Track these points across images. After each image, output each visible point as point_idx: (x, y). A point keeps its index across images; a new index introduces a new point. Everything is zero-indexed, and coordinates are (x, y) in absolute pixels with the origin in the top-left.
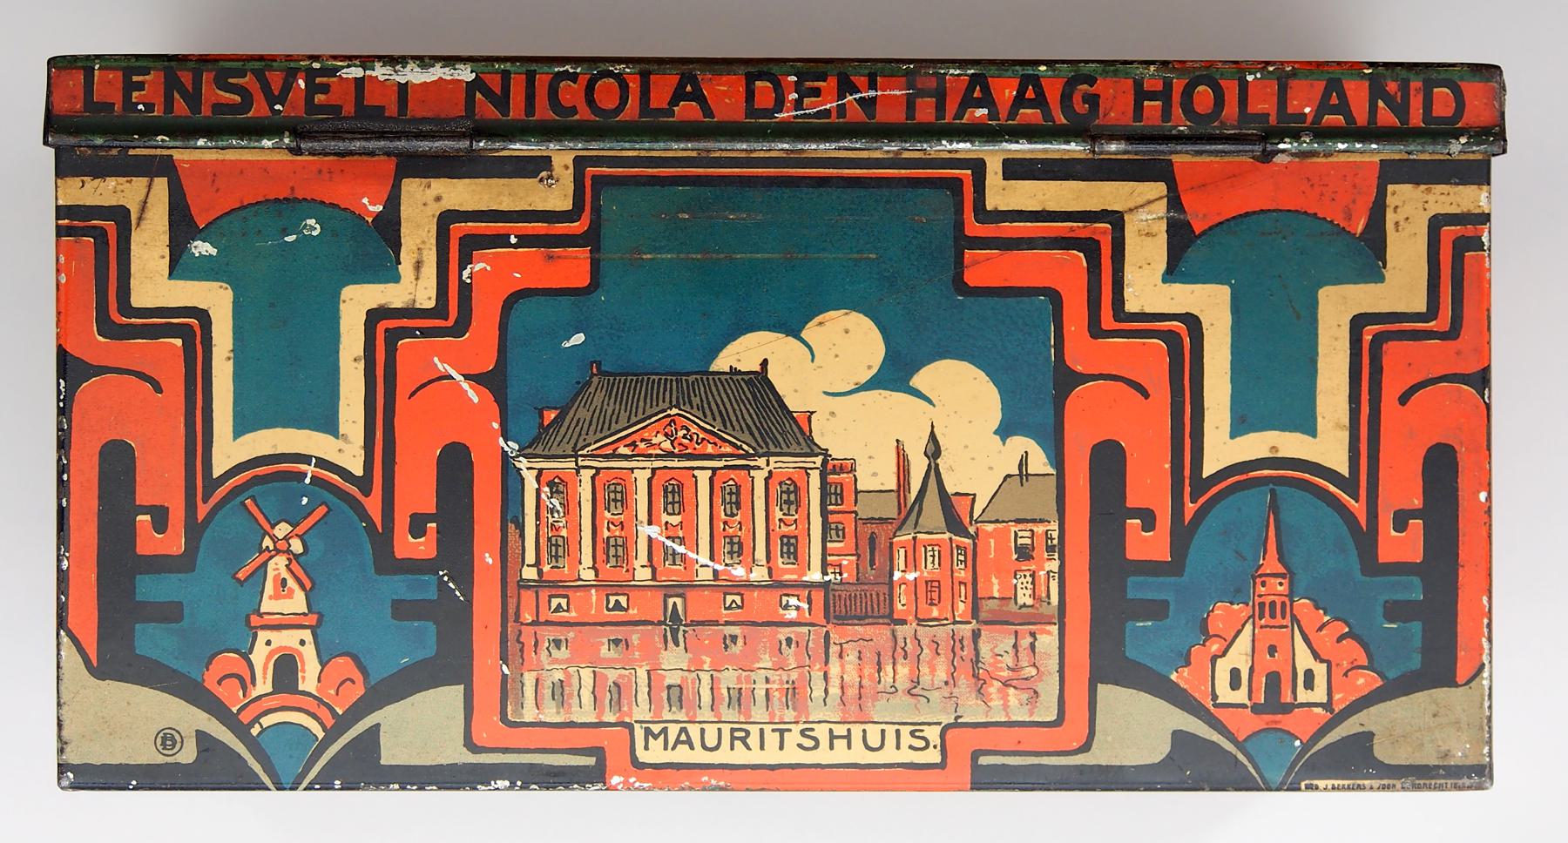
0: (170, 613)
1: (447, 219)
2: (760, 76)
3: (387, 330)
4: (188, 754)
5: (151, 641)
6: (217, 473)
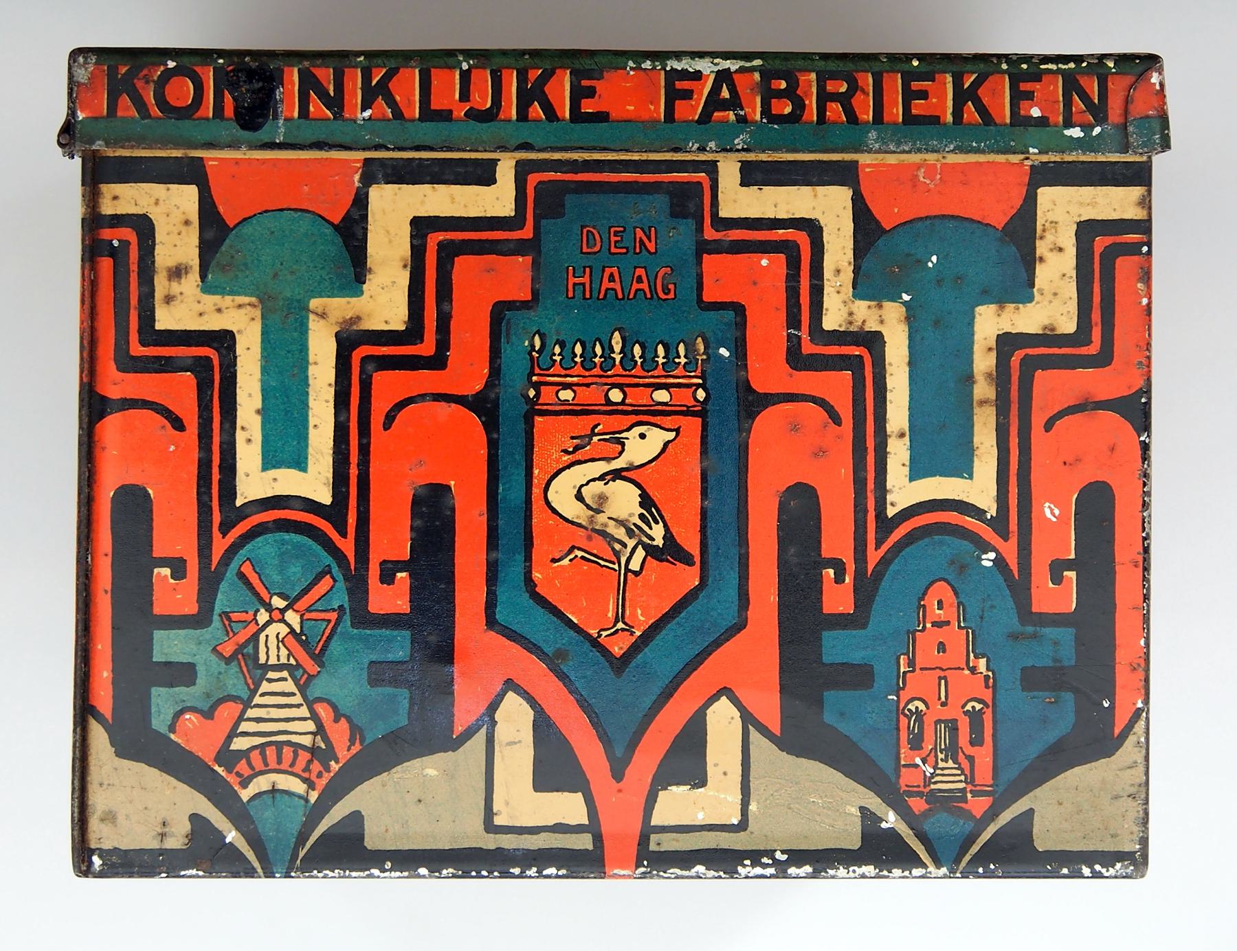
1: (421, 226)
2: (834, 76)
4: (450, 875)
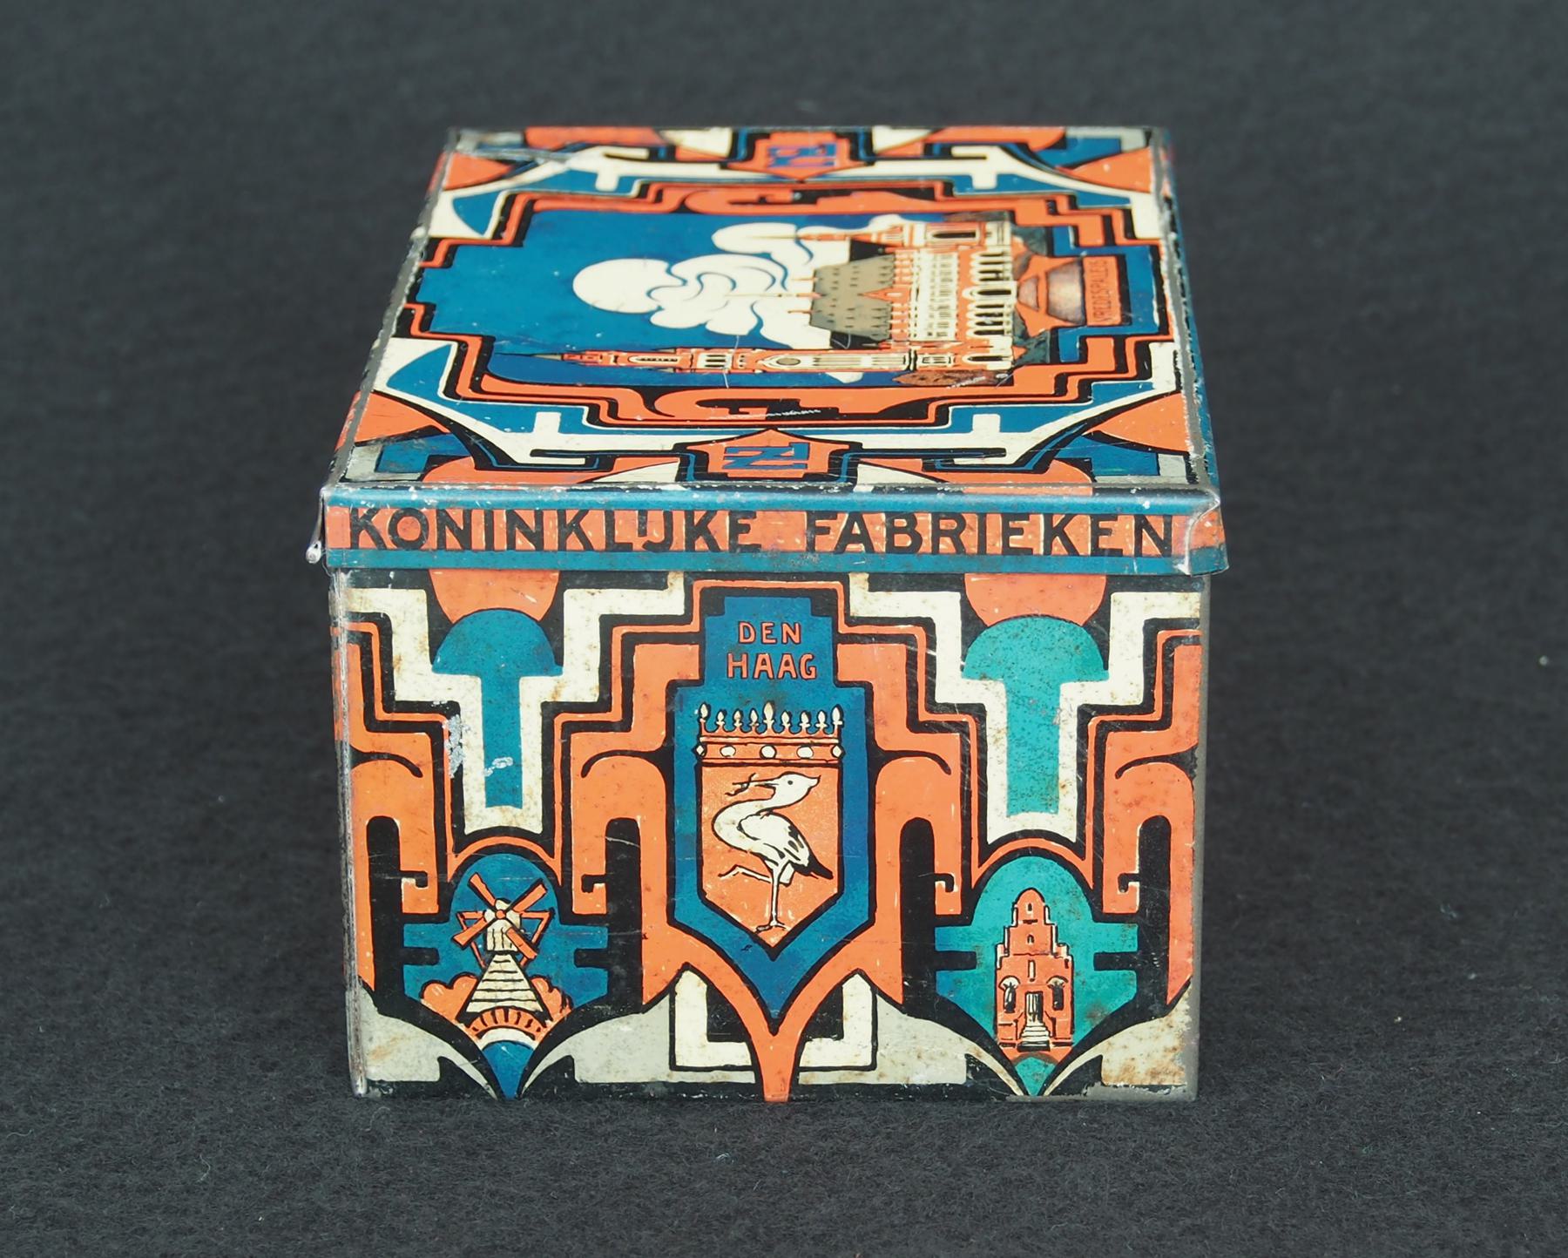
6: (990, 840)
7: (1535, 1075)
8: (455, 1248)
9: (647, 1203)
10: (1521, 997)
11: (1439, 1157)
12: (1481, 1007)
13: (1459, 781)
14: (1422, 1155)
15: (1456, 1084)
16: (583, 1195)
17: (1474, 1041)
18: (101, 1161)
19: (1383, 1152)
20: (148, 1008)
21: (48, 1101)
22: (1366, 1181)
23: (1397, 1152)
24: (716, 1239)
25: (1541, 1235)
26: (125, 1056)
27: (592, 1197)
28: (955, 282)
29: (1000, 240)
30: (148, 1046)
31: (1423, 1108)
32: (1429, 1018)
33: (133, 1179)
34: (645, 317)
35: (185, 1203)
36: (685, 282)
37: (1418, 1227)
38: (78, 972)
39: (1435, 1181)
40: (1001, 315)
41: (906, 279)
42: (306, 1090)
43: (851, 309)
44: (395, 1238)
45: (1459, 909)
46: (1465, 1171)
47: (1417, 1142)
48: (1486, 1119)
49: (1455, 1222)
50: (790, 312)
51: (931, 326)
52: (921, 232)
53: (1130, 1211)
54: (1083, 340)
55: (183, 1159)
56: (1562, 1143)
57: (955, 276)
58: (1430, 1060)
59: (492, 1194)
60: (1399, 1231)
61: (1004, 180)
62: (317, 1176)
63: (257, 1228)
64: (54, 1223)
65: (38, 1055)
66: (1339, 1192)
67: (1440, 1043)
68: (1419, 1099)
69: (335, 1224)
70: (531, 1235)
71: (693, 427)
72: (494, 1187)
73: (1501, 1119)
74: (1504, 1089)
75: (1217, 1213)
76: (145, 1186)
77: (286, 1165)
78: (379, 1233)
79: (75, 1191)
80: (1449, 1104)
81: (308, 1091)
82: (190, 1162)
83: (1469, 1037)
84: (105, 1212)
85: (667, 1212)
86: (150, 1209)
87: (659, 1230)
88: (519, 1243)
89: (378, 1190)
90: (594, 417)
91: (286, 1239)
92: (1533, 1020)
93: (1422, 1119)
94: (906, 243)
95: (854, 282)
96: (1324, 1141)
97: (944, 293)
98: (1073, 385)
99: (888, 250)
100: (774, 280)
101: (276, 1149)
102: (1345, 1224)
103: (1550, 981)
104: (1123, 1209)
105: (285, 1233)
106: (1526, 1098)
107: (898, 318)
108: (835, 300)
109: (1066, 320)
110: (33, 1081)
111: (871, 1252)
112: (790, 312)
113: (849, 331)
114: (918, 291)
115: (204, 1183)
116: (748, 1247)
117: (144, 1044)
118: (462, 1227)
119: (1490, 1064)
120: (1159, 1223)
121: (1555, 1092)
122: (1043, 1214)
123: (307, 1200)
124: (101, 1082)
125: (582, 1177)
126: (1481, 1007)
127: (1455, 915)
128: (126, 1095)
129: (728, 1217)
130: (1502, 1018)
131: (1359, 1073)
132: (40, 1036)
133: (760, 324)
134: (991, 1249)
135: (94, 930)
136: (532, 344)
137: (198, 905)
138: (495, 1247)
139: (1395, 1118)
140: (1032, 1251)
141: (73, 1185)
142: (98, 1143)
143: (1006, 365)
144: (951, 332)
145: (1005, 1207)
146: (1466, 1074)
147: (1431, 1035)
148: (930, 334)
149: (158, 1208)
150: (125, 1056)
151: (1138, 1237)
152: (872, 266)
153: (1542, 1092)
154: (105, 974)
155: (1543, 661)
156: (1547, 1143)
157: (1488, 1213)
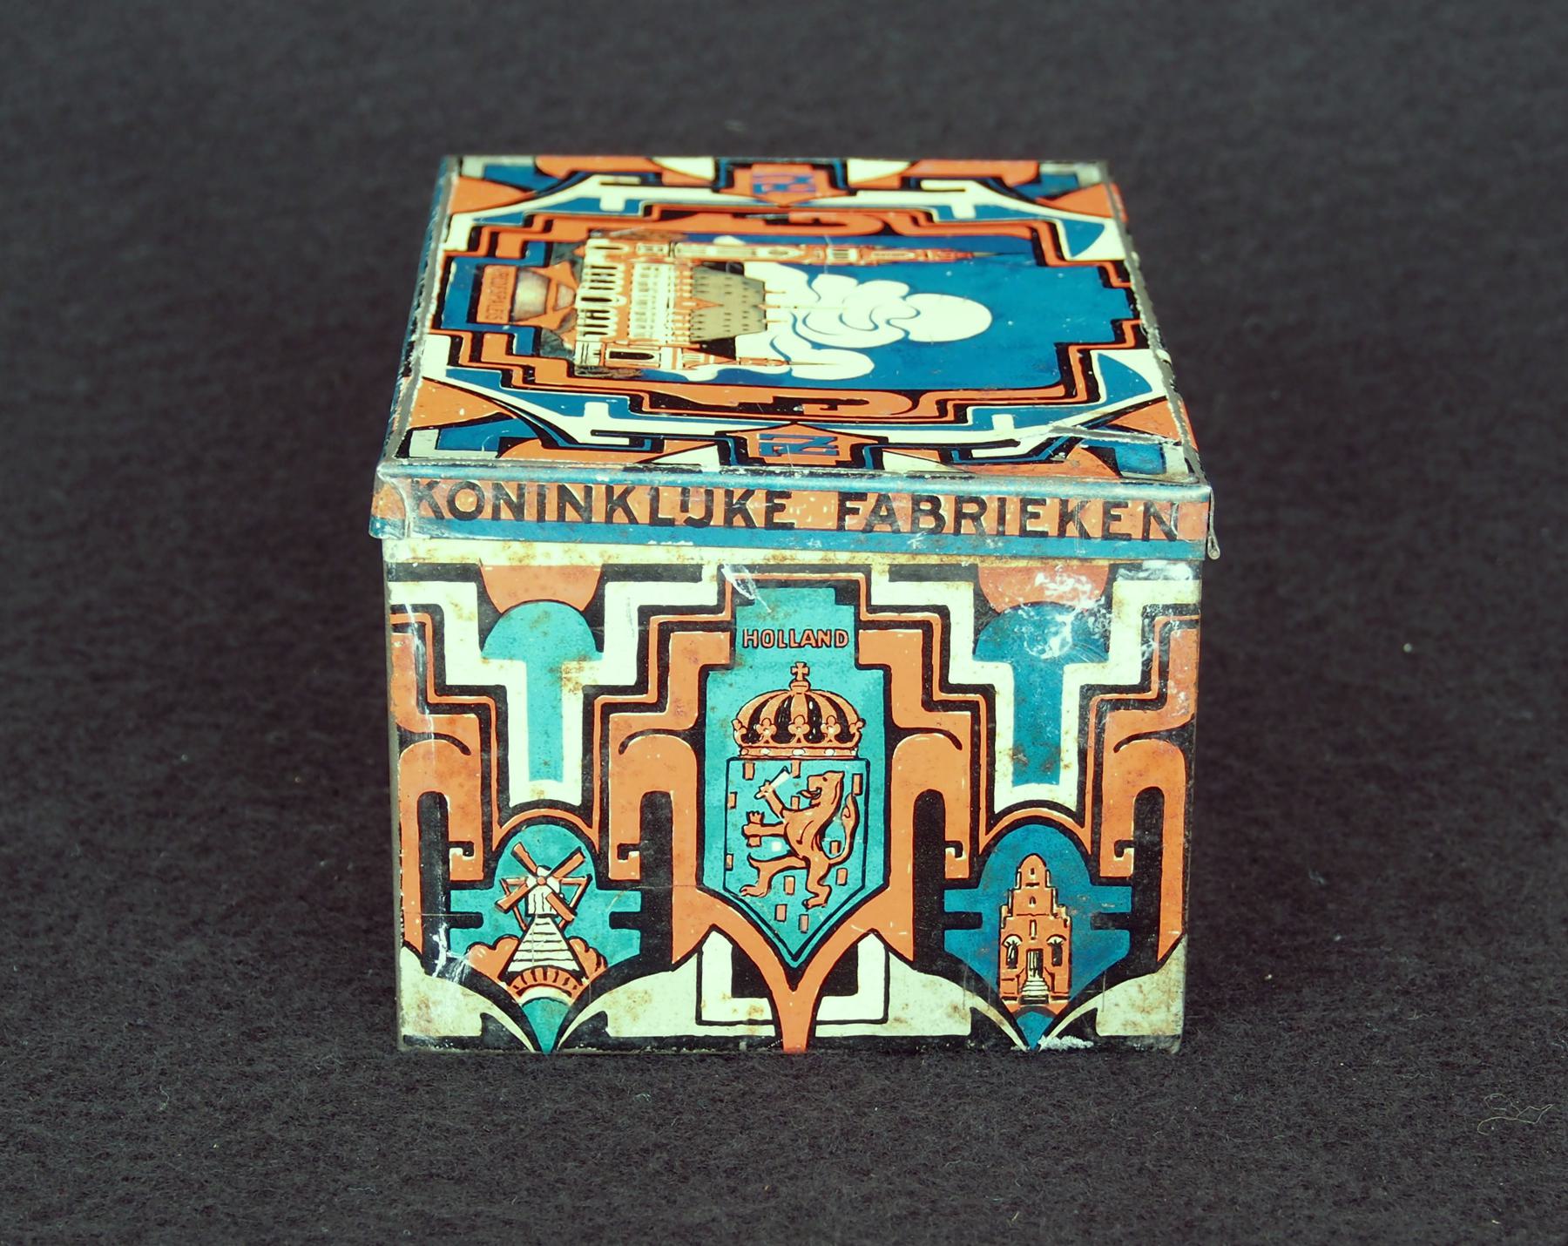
0: (970, 921)
3: (977, 703)
5: (956, 941)
7: (1394, 1030)
8: (395, 1176)
9: (573, 1136)
10: (1382, 958)
11: (1305, 1104)
12: (1346, 967)
13: (1328, 757)
14: (1289, 1103)
15: (1321, 1037)
16: (514, 1128)
17: (1338, 998)
18: (68, 1090)
19: (1252, 1100)
20: (114, 950)
21: (20, 1035)
22: (1237, 1126)
23: (1266, 1099)
24: (635, 1171)
25: (1398, 1177)
26: (92, 994)
27: (522, 1130)
28: (632, 312)
29: (586, 348)
30: (115, 984)
31: (1290, 1059)
32: (1296, 977)
33: (98, 1108)
34: (914, 290)
35: (145, 1131)
36: (888, 322)
37: (1285, 1169)
38: (49, 915)
39: (1300, 1126)
40: (593, 281)
41: (680, 318)
42: (260, 1028)
43: (729, 293)
44: (340, 1166)
45: (1326, 875)
46: (1328, 1118)
47: (1285, 1090)
48: (1349, 1070)
49: (1318, 1165)
50: (784, 293)
51: (656, 276)
52: (666, 362)
53: (1018, 1150)
54: (523, 256)
55: (144, 1090)
56: (1418, 1092)
57: (633, 316)
58: (1297, 1015)
59: (430, 1127)
60: (1266, 1172)
61: (577, 410)
62: (267, 1107)
63: (211, 1155)
64: (24, 1147)
65: (11, 991)
66: (1212, 1136)
67: (1307, 1000)
68: (1288, 1051)
69: (283, 1152)
70: (464, 1164)
71: (845, 209)
72: (431, 1120)
73: (1363, 1071)
74: (1365, 1042)
75: (1099, 1154)
76: (109, 1114)
77: (239, 1096)
78: (324, 1161)
79: (44, 1118)
80: (1315, 1055)
81: (261, 1029)
82: (151, 1093)
83: (1333, 995)
84: (71, 1138)
85: (590, 1146)
86: (113, 1135)
87: (583, 1162)
88: (454, 1171)
89: (325, 1121)
90: (929, 217)
91: (239, 1165)
92: (1393, 979)
93: (1289, 1069)
94: (679, 350)
95: (728, 317)
96: (1199, 1088)
97: (644, 303)
98: (538, 224)
99: (697, 346)
100: (804, 321)
101: (230, 1081)
102: (1216, 1166)
103: (1410, 944)
104: (1012, 1148)
105: (238, 1160)
106: (1386, 1051)
107: (686, 285)
108: (745, 302)
109: (534, 273)
110: (7, 1015)
111: (778, 1185)
112: (784, 293)
113: (729, 275)
114: (668, 306)
115: (163, 1112)
116: (665, 1178)
117: (110, 983)
118: (402, 1156)
119: (1352, 1019)
120: (1045, 1162)
121: (1412, 1046)
122: (938, 1152)
123: (259, 1129)
124: (70, 1017)
125: (513, 1112)
126: (1346, 967)
127: (1322, 881)
128: (93, 1030)
129: (646, 1151)
130: (1365, 977)
131: (1232, 1026)
132: (15, 975)
133: (810, 283)
134: (890, 1184)
135: (66, 876)
136: (1003, 263)
137: (162, 855)
138: (431, 1176)
139: (1265, 1068)
140: (928, 1186)
141: (42, 1112)
142: (67, 1074)
143: (592, 243)
144: (638, 269)
145: (903, 1144)
146: (1331, 1029)
147: (1298, 992)
148: (657, 269)
149: (120, 1134)
150: (92, 994)
151: (1026, 1174)
152: (712, 332)
153: (1400, 1045)
154: (75, 918)
155: (1407, 648)
156: (1405, 1093)
157: (1349, 1158)
